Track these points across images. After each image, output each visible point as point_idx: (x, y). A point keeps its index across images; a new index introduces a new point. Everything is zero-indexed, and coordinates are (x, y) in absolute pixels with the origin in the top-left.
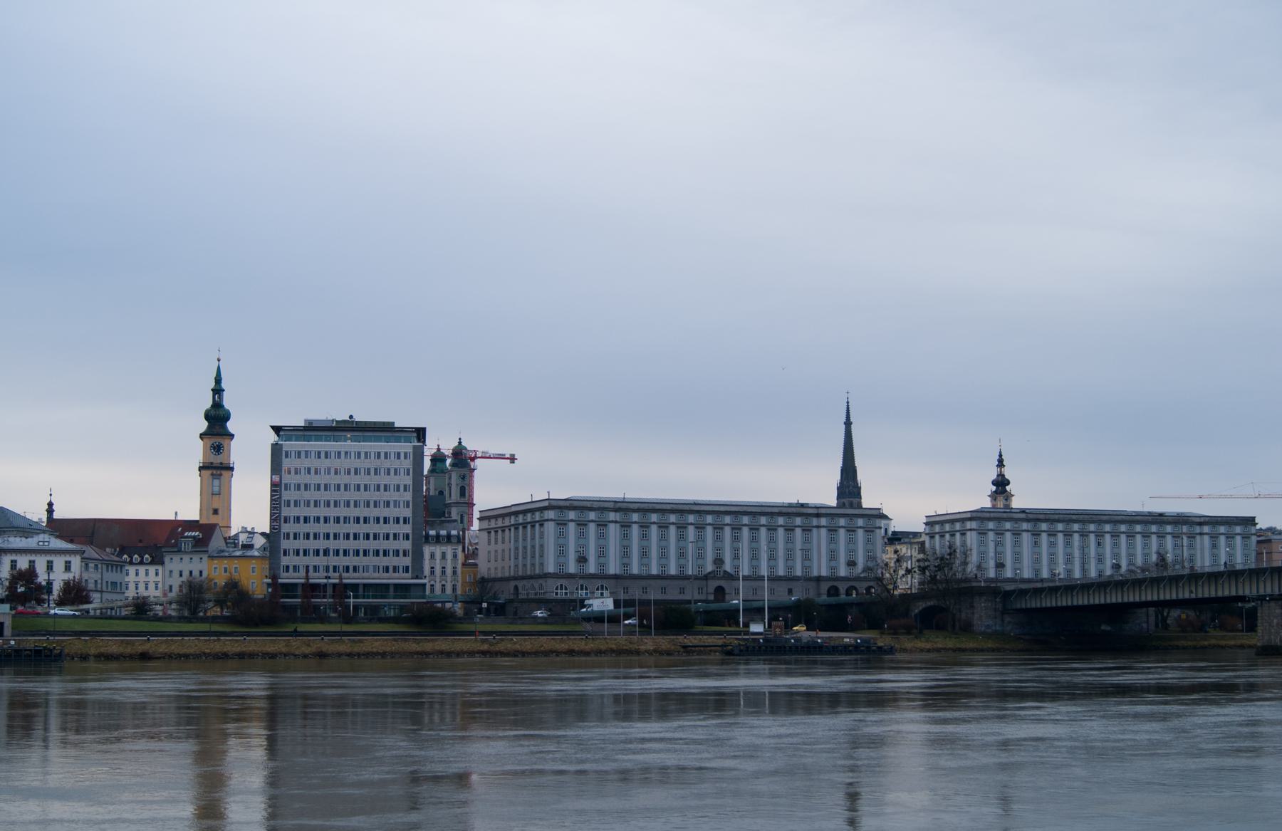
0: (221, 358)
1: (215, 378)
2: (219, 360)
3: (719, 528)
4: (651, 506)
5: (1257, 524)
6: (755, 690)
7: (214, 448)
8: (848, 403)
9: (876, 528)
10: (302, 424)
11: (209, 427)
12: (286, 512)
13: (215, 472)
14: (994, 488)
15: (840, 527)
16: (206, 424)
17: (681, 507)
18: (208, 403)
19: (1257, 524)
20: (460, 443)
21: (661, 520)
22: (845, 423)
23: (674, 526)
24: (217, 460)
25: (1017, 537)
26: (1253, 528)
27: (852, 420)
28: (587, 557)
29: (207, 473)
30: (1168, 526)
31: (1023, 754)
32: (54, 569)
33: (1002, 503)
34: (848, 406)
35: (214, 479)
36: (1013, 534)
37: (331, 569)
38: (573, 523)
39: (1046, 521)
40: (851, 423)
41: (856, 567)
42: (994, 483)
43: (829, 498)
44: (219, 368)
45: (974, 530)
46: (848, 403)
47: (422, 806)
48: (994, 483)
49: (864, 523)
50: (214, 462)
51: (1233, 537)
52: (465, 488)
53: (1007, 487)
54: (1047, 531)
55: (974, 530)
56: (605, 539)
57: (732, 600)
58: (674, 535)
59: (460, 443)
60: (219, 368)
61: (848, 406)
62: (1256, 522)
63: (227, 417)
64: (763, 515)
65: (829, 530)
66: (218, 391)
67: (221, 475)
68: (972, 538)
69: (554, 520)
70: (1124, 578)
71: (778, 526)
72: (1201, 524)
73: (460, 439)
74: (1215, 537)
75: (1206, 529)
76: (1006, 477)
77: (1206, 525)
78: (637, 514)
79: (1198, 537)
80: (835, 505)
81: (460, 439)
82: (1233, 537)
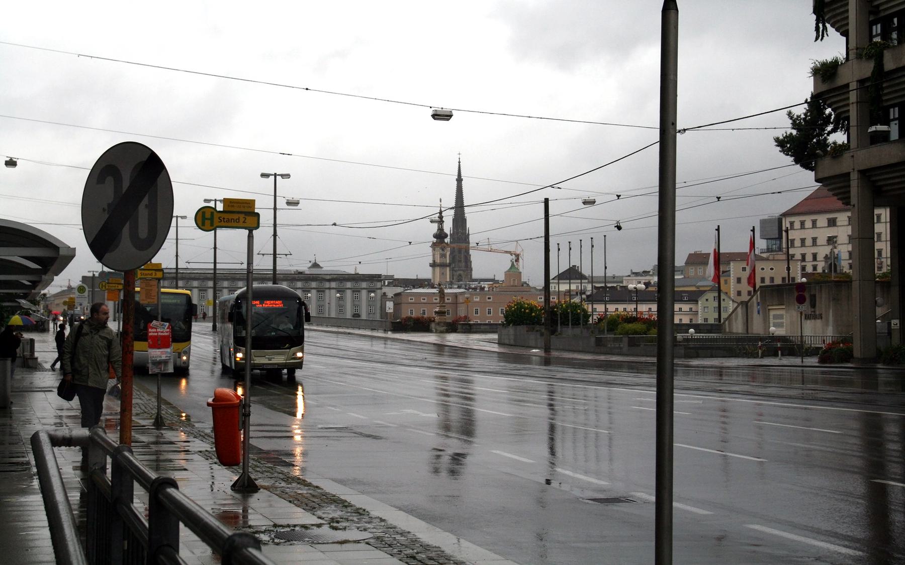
6: (582, 370)
8: (459, 162)
14: (435, 240)
15: (312, 289)
22: (457, 180)
28: (360, 314)
31: (735, 378)
34: (459, 165)
36: (303, 291)
38: (568, 288)
39: (227, 279)
40: (462, 180)
41: (353, 314)
45: (333, 288)
46: (459, 162)
47: (460, 420)
48: (435, 236)
49: (228, 284)
51: (359, 291)
56: (343, 300)
58: (350, 298)
61: (459, 165)
68: (312, 295)
70: (245, 318)
72: (329, 280)
74: (321, 291)
76: (71, 247)
77: (333, 281)
79: (327, 291)
82: (359, 291)
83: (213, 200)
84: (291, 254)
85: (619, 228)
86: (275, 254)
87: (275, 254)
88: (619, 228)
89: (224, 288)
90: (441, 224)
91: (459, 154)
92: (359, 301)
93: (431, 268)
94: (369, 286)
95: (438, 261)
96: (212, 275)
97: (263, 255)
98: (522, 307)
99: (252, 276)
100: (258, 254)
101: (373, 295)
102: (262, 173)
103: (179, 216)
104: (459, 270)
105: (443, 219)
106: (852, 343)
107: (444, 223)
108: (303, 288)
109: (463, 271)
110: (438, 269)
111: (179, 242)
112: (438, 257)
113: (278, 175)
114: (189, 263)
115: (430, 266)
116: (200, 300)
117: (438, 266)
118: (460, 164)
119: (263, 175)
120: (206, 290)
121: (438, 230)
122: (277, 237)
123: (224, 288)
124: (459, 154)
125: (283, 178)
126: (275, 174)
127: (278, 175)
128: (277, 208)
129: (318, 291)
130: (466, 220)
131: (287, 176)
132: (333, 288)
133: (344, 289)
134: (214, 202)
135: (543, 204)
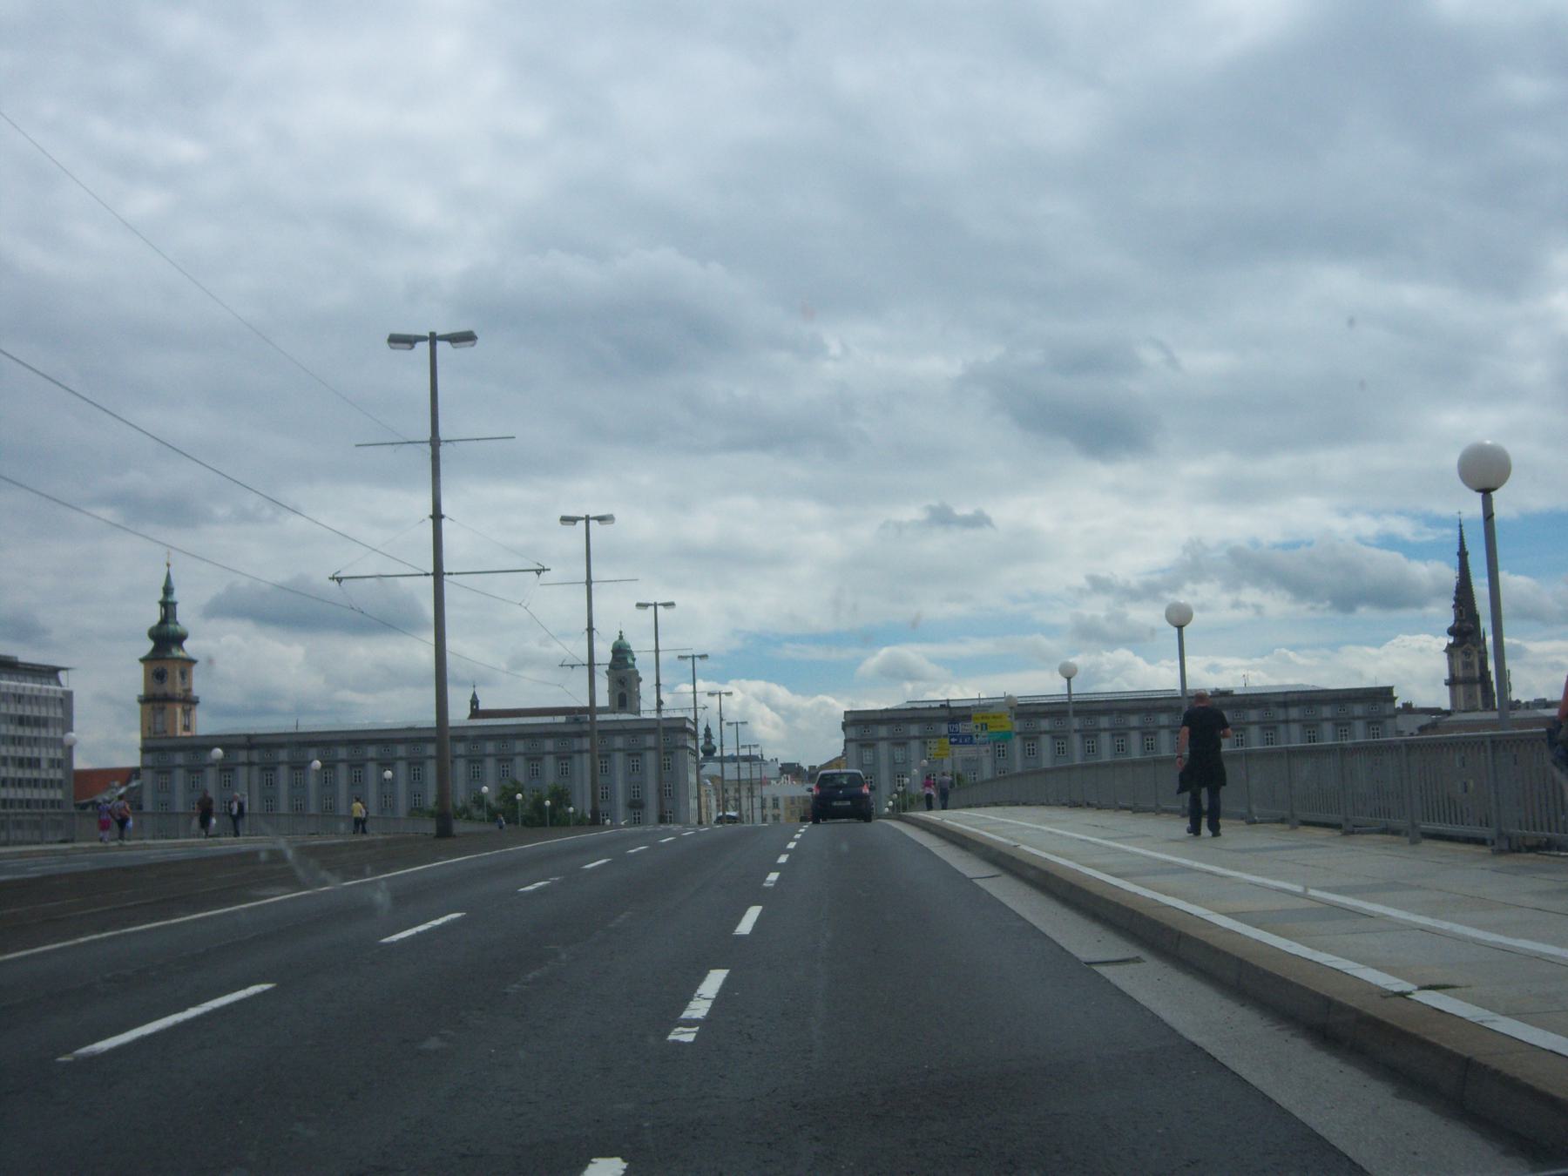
0: (170, 563)
1: (164, 589)
2: (168, 565)
3: (1271, 728)
5: (1396, 698)
9: (677, 747)
11: (155, 650)
17: (382, 736)
18: (154, 616)
19: (1396, 698)
20: (621, 637)
21: (862, 735)
22: (1458, 554)
23: (552, 756)
24: (159, 690)
26: (1388, 705)
27: (1468, 548)
29: (149, 706)
37: (769, 803)
40: (1467, 554)
43: (587, 704)
44: (168, 576)
45: (1294, 721)
52: (625, 695)
59: (621, 637)
60: (168, 576)
62: (1395, 695)
66: (168, 607)
69: (624, 750)
71: (1041, 733)
73: (621, 632)
75: (1294, 713)
78: (522, 742)
79: (577, 757)
80: (1188, 688)
81: (621, 632)
82: (1349, 724)
83: (582, 519)
92: (1067, 756)
93: (1448, 687)
94: (1085, 726)
95: (1460, 674)
96: (1067, 697)
97: (572, 666)
98: (567, 795)
99: (603, 710)
100: (562, 666)
101: (388, 774)
108: (1112, 729)
110: (1460, 689)
115: (1446, 684)
116: (1056, 756)
118: (1463, 528)
121: (1455, 621)
122: (595, 633)
123: (1100, 730)
127: (660, 605)
128: (446, 570)
129: (629, 755)
130: (1478, 616)
131: (467, 338)
132: (1294, 721)
133: (1095, 730)
134: (583, 522)
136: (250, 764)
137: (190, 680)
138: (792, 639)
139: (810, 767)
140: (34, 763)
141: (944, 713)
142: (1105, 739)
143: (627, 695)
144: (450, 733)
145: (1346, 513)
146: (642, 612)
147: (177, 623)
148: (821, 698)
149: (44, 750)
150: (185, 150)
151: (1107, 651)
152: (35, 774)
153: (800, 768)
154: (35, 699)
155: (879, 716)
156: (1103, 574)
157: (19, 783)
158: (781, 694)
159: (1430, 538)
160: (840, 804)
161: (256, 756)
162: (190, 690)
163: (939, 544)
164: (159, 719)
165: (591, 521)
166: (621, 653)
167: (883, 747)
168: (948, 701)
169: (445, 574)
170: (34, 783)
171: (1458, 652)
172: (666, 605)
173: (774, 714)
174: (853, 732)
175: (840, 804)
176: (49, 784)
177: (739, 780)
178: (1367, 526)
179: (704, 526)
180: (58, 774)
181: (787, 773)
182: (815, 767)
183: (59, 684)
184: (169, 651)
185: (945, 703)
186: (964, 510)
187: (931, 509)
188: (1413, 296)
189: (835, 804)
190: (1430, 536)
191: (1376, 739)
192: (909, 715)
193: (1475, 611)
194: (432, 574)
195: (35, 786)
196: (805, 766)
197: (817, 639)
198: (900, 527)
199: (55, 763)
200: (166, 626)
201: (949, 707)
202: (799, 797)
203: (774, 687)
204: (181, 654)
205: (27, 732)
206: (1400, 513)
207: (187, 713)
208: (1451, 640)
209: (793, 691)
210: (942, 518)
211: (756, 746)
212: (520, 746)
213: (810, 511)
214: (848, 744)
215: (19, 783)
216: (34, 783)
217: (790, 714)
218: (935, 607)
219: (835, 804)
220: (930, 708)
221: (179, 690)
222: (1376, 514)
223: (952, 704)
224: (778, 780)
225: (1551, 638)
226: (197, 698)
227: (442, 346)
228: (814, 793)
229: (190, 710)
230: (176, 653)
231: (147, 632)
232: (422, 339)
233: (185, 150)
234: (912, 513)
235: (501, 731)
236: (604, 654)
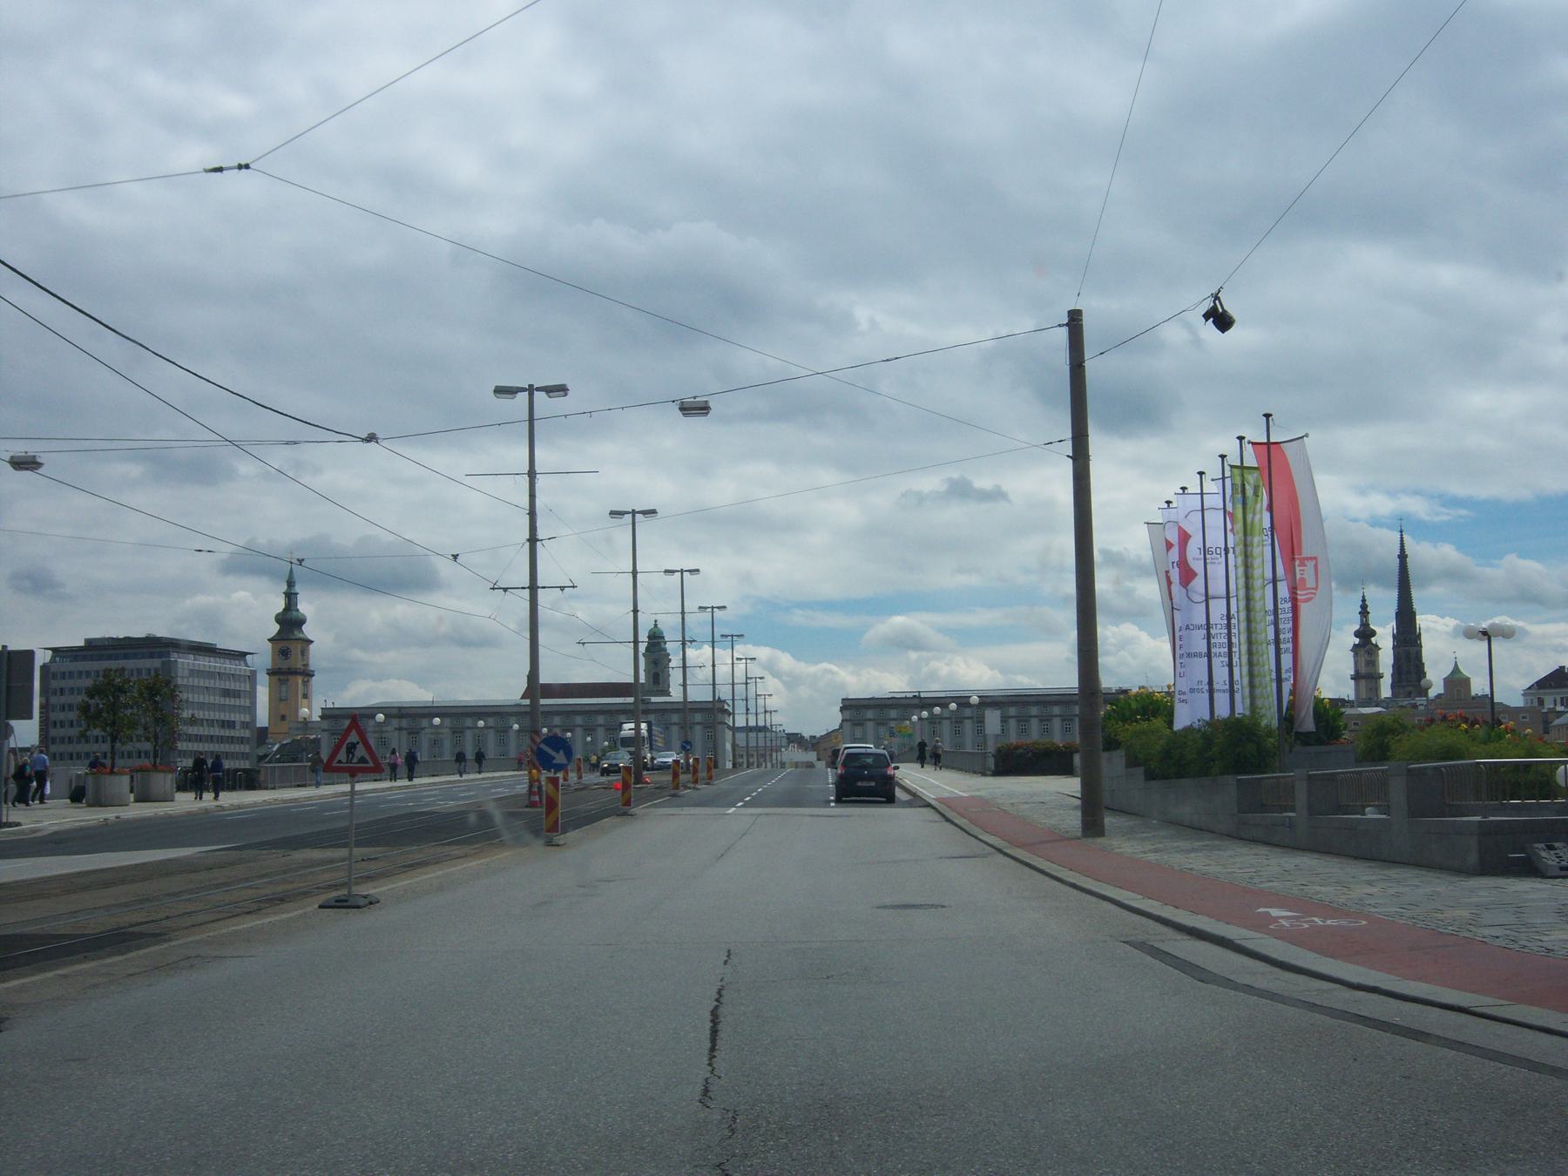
4: (492, 710)
7: (286, 655)
10: (82, 644)
12: (53, 732)
13: (282, 678)
14: (1357, 641)
16: (277, 627)
20: (656, 625)
24: (284, 665)
25: (414, 736)
30: (696, 714)
32: (1165, 906)
33: (1363, 659)
35: (281, 685)
42: (1357, 634)
48: (1357, 634)
50: (283, 667)
52: (658, 674)
53: (1372, 639)
54: (1016, 717)
55: (491, 727)
57: (1259, 908)
59: (656, 625)
63: (300, 622)
64: (623, 714)
65: (585, 730)
67: (288, 680)
69: (874, 720)
81: (656, 621)
84: (574, 587)
85: (1222, 321)
86: (533, 588)
87: (533, 588)
88: (1222, 321)
89: (1031, 717)
90: (1365, 617)
91: (1401, 519)
95: (1363, 671)
97: (505, 590)
102: (497, 387)
103: (685, 569)
104: (1408, 685)
105: (1368, 609)
106: (111, 670)
107: (1370, 615)
109: (1413, 686)
110: (1363, 682)
111: (686, 617)
112: (1363, 665)
113: (539, 389)
114: (583, 644)
115: (1352, 679)
117: (1363, 677)
119: (500, 391)
120: (1027, 721)
124: (1401, 519)
125: (550, 397)
126: (531, 386)
127: (539, 389)
131: (561, 390)
135: (1064, 331)
136: (400, 729)
137: (308, 658)
138: (801, 605)
139: (811, 737)
140: (230, 725)
141: (916, 701)
142: (1034, 723)
143: (660, 674)
144: (541, 709)
145: (1362, 491)
146: (505, 402)
147: (298, 610)
148: (825, 665)
149: (238, 715)
150: (233, 104)
151: (1113, 626)
152: (232, 733)
153: (802, 737)
154: (234, 677)
155: (866, 702)
156: (1115, 549)
157: (221, 739)
158: (786, 661)
159: (1445, 518)
160: (865, 784)
161: (404, 723)
162: (307, 665)
163: (956, 514)
164: (284, 688)
165: (637, 515)
166: (656, 639)
167: (870, 725)
168: (919, 692)
169: (539, 587)
170: (231, 740)
171: (1362, 651)
172: (550, 390)
173: (776, 680)
174: (848, 714)
175: (865, 784)
176: (242, 740)
177: (757, 747)
178: (1383, 505)
179: (722, 491)
180: (247, 733)
181: (793, 742)
182: (814, 737)
183: (247, 665)
184: (292, 632)
185: (917, 694)
186: (983, 483)
187: (952, 482)
188: (1449, 276)
189: (860, 784)
190: (1445, 515)
191: (560, 787)
192: (890, 702)
193: (1412, 608)
194: (528, 588)
195: (212, 741)
196: (806, 735)
197: (829, 606)
198: (921, 498)
199: (245, 725)
200: (289, 613)
201: (919, 698)
202: (802, 762)
203: (778, 653)
204: (301, 635)
205: (227, 701)
206: (1416, 492)
207: (306, 683)
208: (1357, 641)
209: (798, 657)
210: (960, 490)
211: (781, 725)
212: (1056, 710)
213: (827, 477)
214: (845, 723)
215: (221, 739)
216: (231, 740)
217: (792, 682)
218: (944, 577)
219: (860, 784)
220: (906, 698)
221: (299, 665)
222: (1392, 493)
223: (922, 695)
224: (787, 747)
225: (1554, 621)
226: (313, 671)
227: (638, 516)
228: (839, 771)
229: (308, 681)
230: (298, 635)
231: (274, 616)
232: (628, 513)
233: (233, 104)
234: (930, 483)
235: (587, 708)
236: (643, 637)
